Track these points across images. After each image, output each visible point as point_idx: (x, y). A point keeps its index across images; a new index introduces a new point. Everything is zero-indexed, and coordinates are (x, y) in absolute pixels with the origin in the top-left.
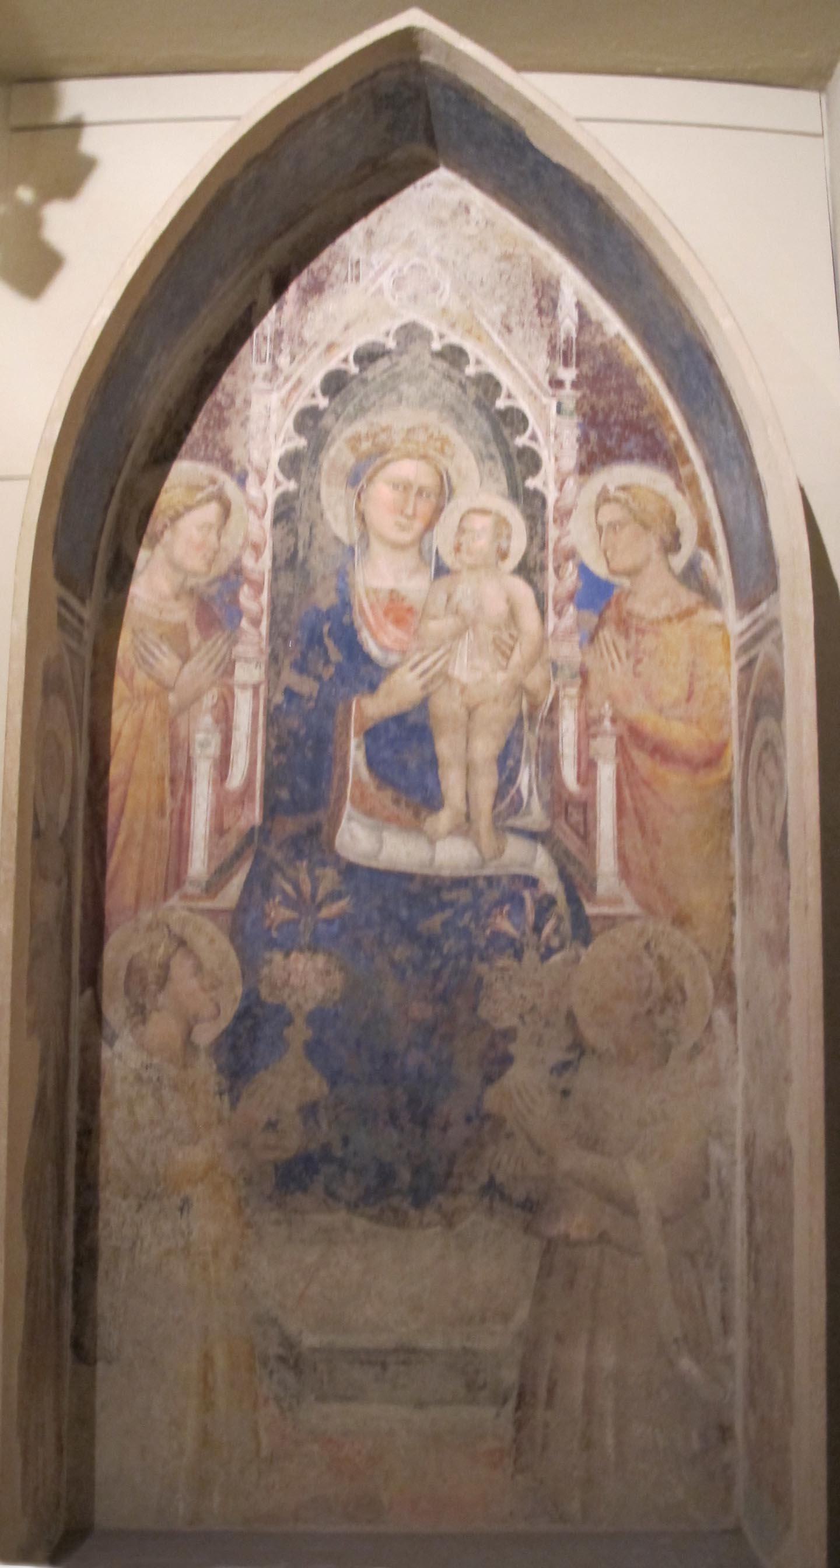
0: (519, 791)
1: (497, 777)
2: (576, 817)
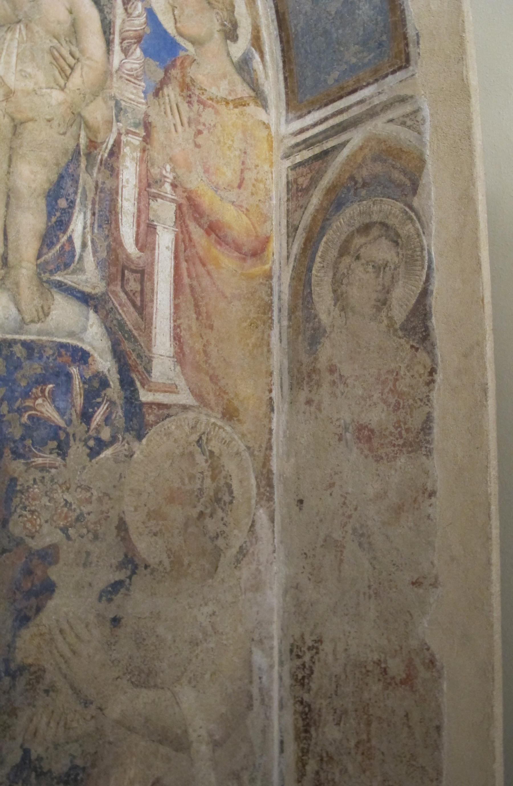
0: (70, 240)
1: (44, 219)
2: (133, 285)
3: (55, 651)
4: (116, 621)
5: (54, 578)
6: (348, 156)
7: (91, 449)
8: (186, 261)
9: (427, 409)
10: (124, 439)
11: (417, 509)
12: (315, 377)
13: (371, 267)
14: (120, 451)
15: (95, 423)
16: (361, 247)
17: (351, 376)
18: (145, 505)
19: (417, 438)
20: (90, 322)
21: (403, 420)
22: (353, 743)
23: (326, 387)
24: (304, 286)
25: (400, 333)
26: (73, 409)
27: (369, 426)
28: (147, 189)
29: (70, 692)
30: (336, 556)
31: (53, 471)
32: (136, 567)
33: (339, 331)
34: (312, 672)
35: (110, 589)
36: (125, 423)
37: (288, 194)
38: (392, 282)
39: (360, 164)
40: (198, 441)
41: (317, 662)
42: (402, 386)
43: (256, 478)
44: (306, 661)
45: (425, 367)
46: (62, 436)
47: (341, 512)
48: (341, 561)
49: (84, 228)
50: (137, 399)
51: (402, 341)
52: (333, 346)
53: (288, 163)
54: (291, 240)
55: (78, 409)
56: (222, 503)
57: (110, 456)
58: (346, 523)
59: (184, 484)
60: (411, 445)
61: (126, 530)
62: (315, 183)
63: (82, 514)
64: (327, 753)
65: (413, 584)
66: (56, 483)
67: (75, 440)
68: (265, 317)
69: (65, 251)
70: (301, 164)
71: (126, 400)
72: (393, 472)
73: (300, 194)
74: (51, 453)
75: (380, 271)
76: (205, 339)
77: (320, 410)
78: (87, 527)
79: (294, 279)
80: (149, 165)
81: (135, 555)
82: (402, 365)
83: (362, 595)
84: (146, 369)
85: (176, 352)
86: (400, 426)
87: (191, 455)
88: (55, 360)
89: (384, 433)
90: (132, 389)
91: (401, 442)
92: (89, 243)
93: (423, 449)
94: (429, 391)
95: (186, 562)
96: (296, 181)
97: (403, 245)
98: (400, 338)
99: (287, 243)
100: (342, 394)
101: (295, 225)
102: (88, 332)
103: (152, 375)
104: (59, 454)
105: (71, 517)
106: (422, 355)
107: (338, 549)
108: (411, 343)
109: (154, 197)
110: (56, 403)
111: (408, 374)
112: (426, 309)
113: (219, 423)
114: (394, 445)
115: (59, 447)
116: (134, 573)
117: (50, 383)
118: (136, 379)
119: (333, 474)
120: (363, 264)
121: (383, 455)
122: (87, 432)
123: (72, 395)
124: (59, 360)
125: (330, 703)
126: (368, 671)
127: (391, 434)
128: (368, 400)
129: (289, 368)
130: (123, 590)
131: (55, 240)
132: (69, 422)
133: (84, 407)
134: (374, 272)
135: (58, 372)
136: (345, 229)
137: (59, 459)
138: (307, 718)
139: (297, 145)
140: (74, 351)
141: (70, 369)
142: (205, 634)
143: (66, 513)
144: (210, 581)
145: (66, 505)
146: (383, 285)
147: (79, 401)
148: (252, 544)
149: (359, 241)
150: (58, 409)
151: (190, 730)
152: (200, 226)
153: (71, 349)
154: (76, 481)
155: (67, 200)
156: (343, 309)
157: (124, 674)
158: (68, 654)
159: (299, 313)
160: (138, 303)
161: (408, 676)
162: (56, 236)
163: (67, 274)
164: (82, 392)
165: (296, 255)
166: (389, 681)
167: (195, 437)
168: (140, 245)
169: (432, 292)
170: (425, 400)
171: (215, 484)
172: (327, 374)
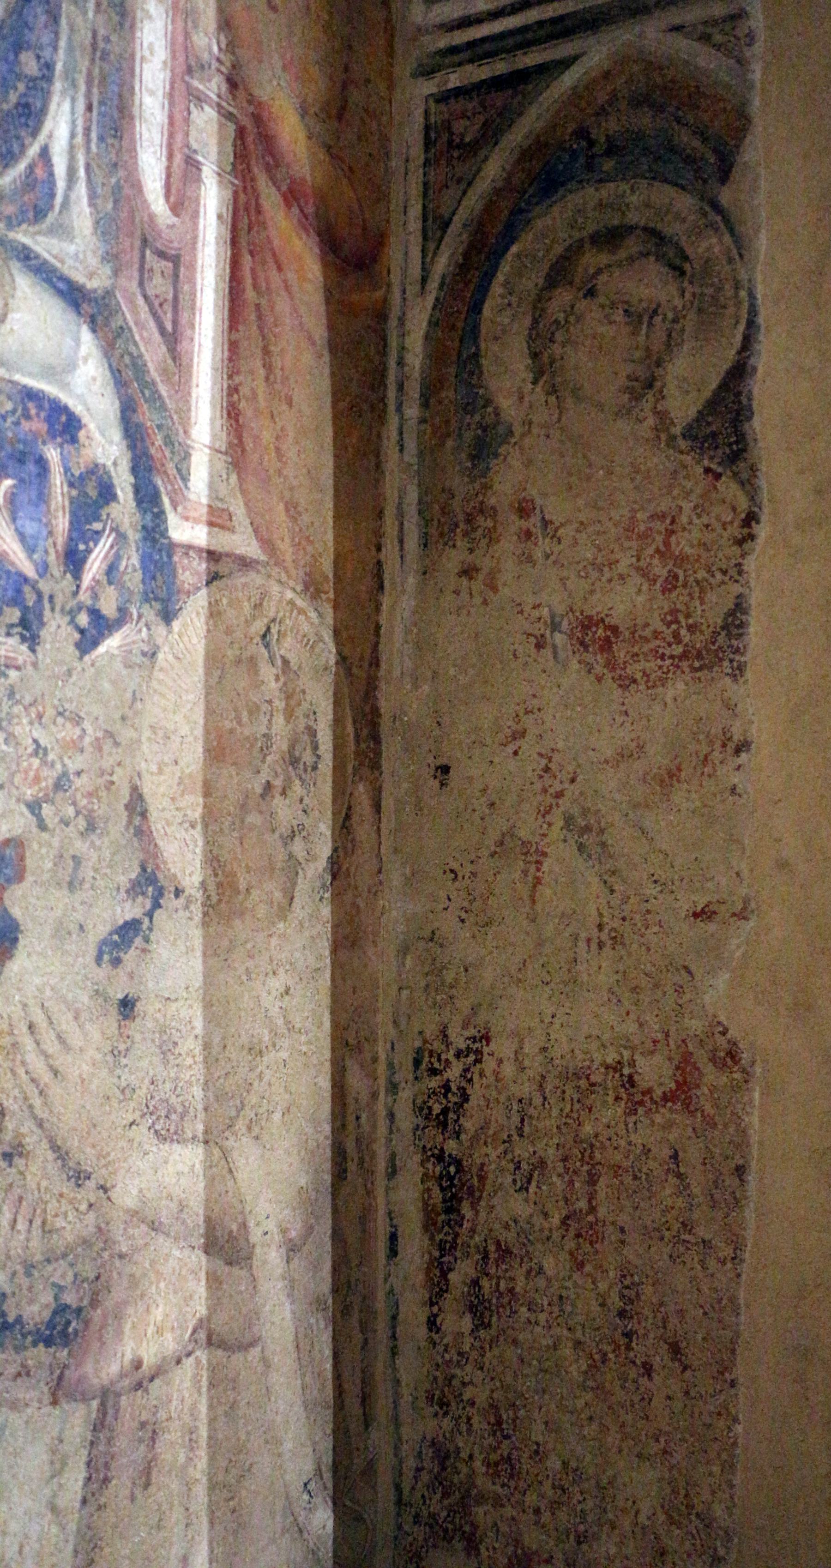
0: (45, 154)
2: (159, 285)
3: (21, 1071)
4: (127, 1006)
5: (16, 912)
6: (574, 88)
7: (82, 632)
8: (251, 253)
9: (736, 589)
10: (140, 617)
11: (710, 776)
12: (485, 523)
13: (621, 312)
14: (134, 642)
15: (90, 575)
16: (599, 271)
17: (568, 522)
18: (176, 763)
19: (713, 643)
20: (84, 350)
21: (682, 607)
22: (556, 1220)
23: (508, 545)
24: (461, 341)
25: (683, 444)
26: (50, 541)
27: (607, 620)
28: (187, 78)
29: (50, 1155)
30: (525, 873)
31: (13, 674)
32: (160, 892)
33: (543, 432)
34: (465, 1098)
35: (116, 937)
36: (143, 581)
37: (426, 151)
38: (668, 345)
39: (603, 108)
40: (264, 636)
41: (476, 1078)
42: (682, 544)
43: (354, 722)
44: (452, 1078)
45: (734, 509)
46: (30, 599)
47: (538, 786)
48: (538, 881)
49: (73, 135)
50: (164, 534)
51: (688, 459)
52: (528, 464)
53: (429, 87)
54: (432, 246)
55: (60, 541)
56: (301, 766)
57: (116, 652)
58: (551, 806)
59: (239, 723)
60: (699, 656)
61: (144, 815)
62: (495, 134)
63: (65, 774)
64: (498, 1243)
65: (696, 915)
66: (18, 702)
67: (53, 609)
68: (373, 397)
69: (36, 179)
70: (458, 92)
71: (144, 533)
72: (657, 708)
73: (456, 154)
74: (8, 634)
75: (640, 322)
76: (279, 425)
77: (495, 589)
78: (74, 803)
79: (437, 324)
80: (190, 24)
81: (158, 867)
82: (684, 504)
83: (582, 944)
84: (179, 470)
85: (230, 444)
86: (677, 622)
87: (252, 661)
88: (17, 423)
89: (640, 632)
90: (155, 510)
91: (678, 650)
92: (82, 173)
93: (726, 663)
94: (743, 556)
95: (242, 886)
96: (447, 126)
97: (693, 276)
98: (682, 452)
99: (424, 251)
100: (547, 557)
101: (441, 217)
102: (78, 372)
103: (190, 484)
104: (23, 639)
105: (46, 779)
106: (728, 488)
107: (529, 858)
108: (706, 462)
109: (199, 99)
110: (19, 522)
111: (696, 521)
112: (740, 402)
113: (300, 602)
114: (663, 657)
115: (24, 623)
116: (157, 905)
117: (7, 476)
118: (162, 489)
119: (521, 714)
120: (602, 306)
121: (638, 676)
122: (76, 593)
123: (49, 507)
124: (26, 425)
125: (505, 1152)
126: (593, 1085)
127: (656, 634)
128: (606, 569)
129: (420, 502)
130: (138, 941)
131: (16, 148)
132: (43, 569)
133: (71, 539)
134: (627, 324)
135: (24, 453)
136: (563, 235)
137: (24, 648)
138: (452, 1185)
139: (453, 50)
140: (51, 409)
141: (45, 449)
142: (274, 1033)
143: (37, 770)
144: (281, 925)
145: (36, 753)
146: (647, 349)
147: (62, 523)
148: (346, 853)
149: (592, 259)
150: (22, 537)
151: (251, 1224)
152: (274, 184)
153: (47, 406)
154: (56, 702)
155: (38, 57)
156: (553, 390)
157: (143, 1116)
158: (46, 1077)
159: (448, 394)
160: (169, 327)
161: (682, 1085)
162: (18, 138)
163: (39, 233)
164: (67, 503)
165: (444, 277)
166: (638, 1097)
167: (259, 626)
168: (172, 199)
169: (755, 369)
170: (733, 572)
171: (290, 726)
172: (514, 517)
